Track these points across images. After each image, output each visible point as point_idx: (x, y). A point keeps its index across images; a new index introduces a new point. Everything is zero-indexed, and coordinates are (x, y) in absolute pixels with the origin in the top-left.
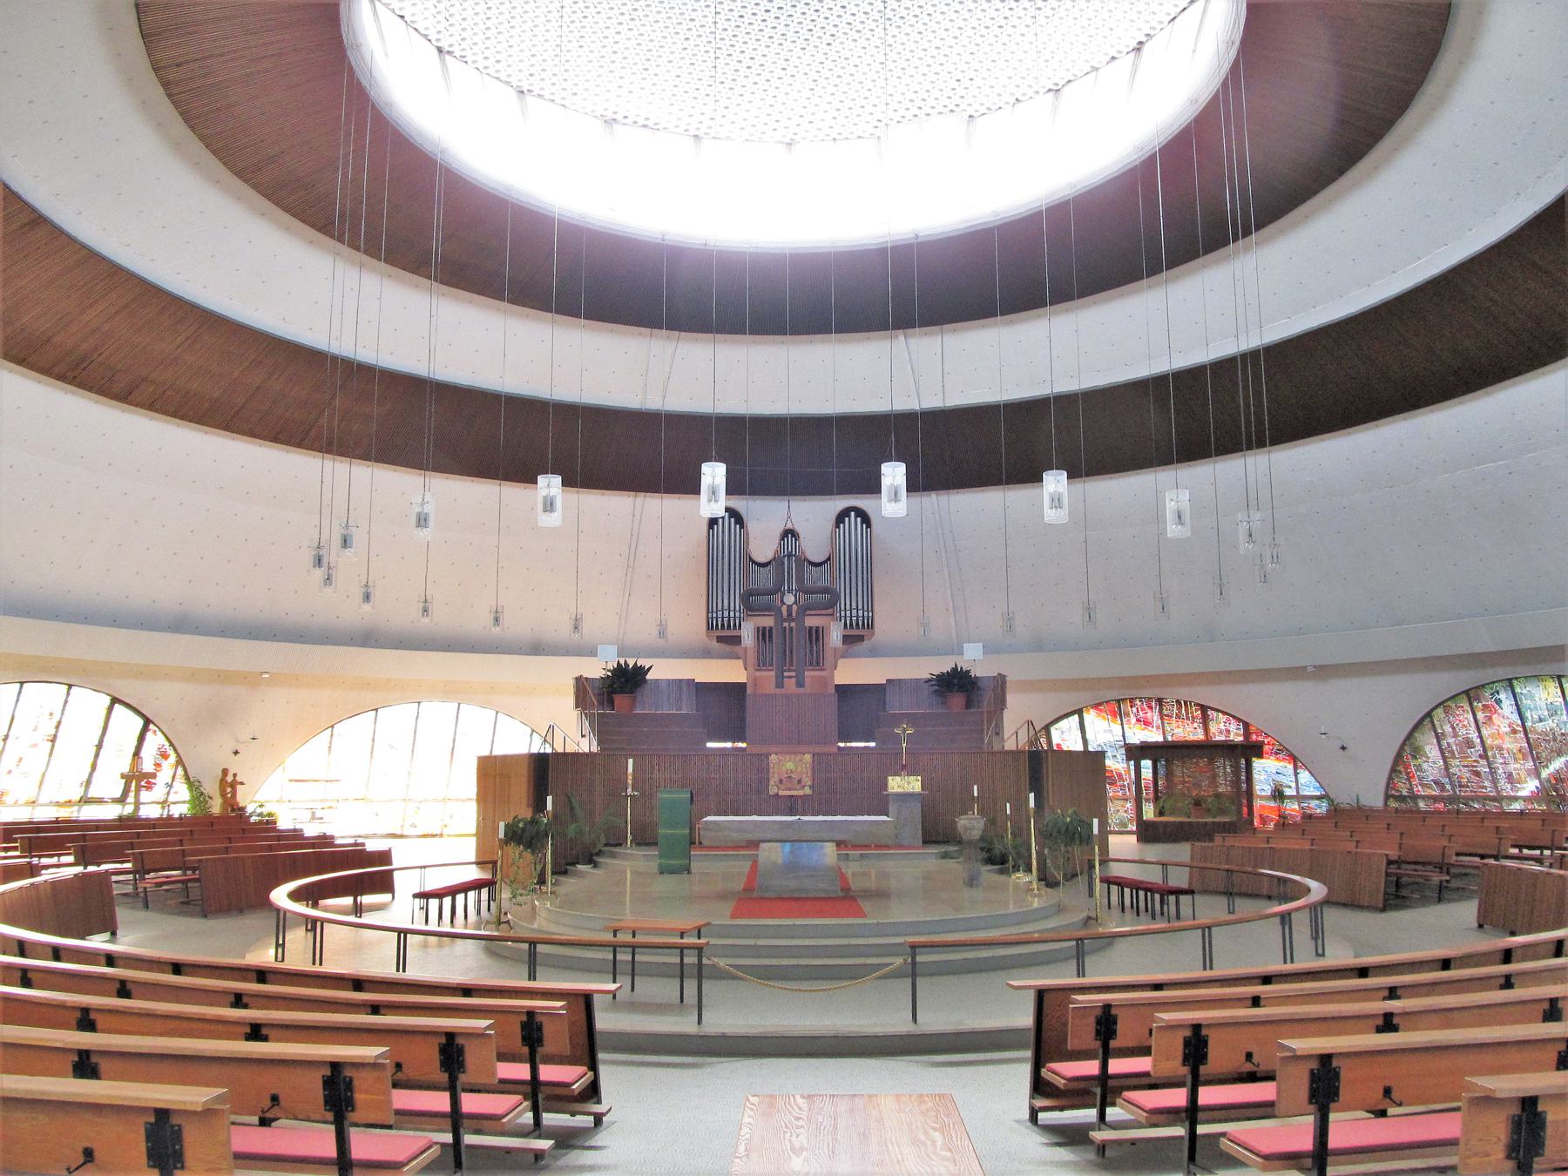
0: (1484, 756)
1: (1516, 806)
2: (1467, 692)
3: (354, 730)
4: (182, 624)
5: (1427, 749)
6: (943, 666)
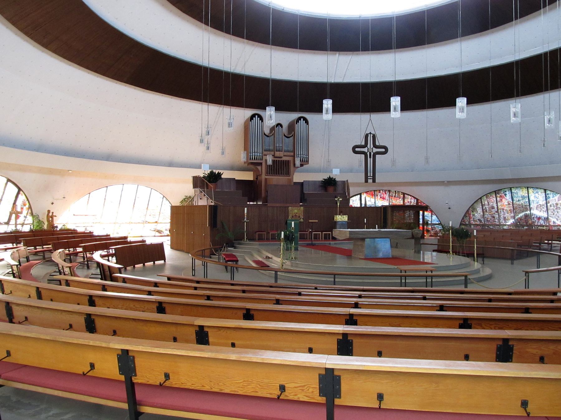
0: (497, 212)
1: (505, 227)
2: (495, 191)
3: (98, 195)
4: (40, 148)
5: (478, 209)
6: (326, 176)
